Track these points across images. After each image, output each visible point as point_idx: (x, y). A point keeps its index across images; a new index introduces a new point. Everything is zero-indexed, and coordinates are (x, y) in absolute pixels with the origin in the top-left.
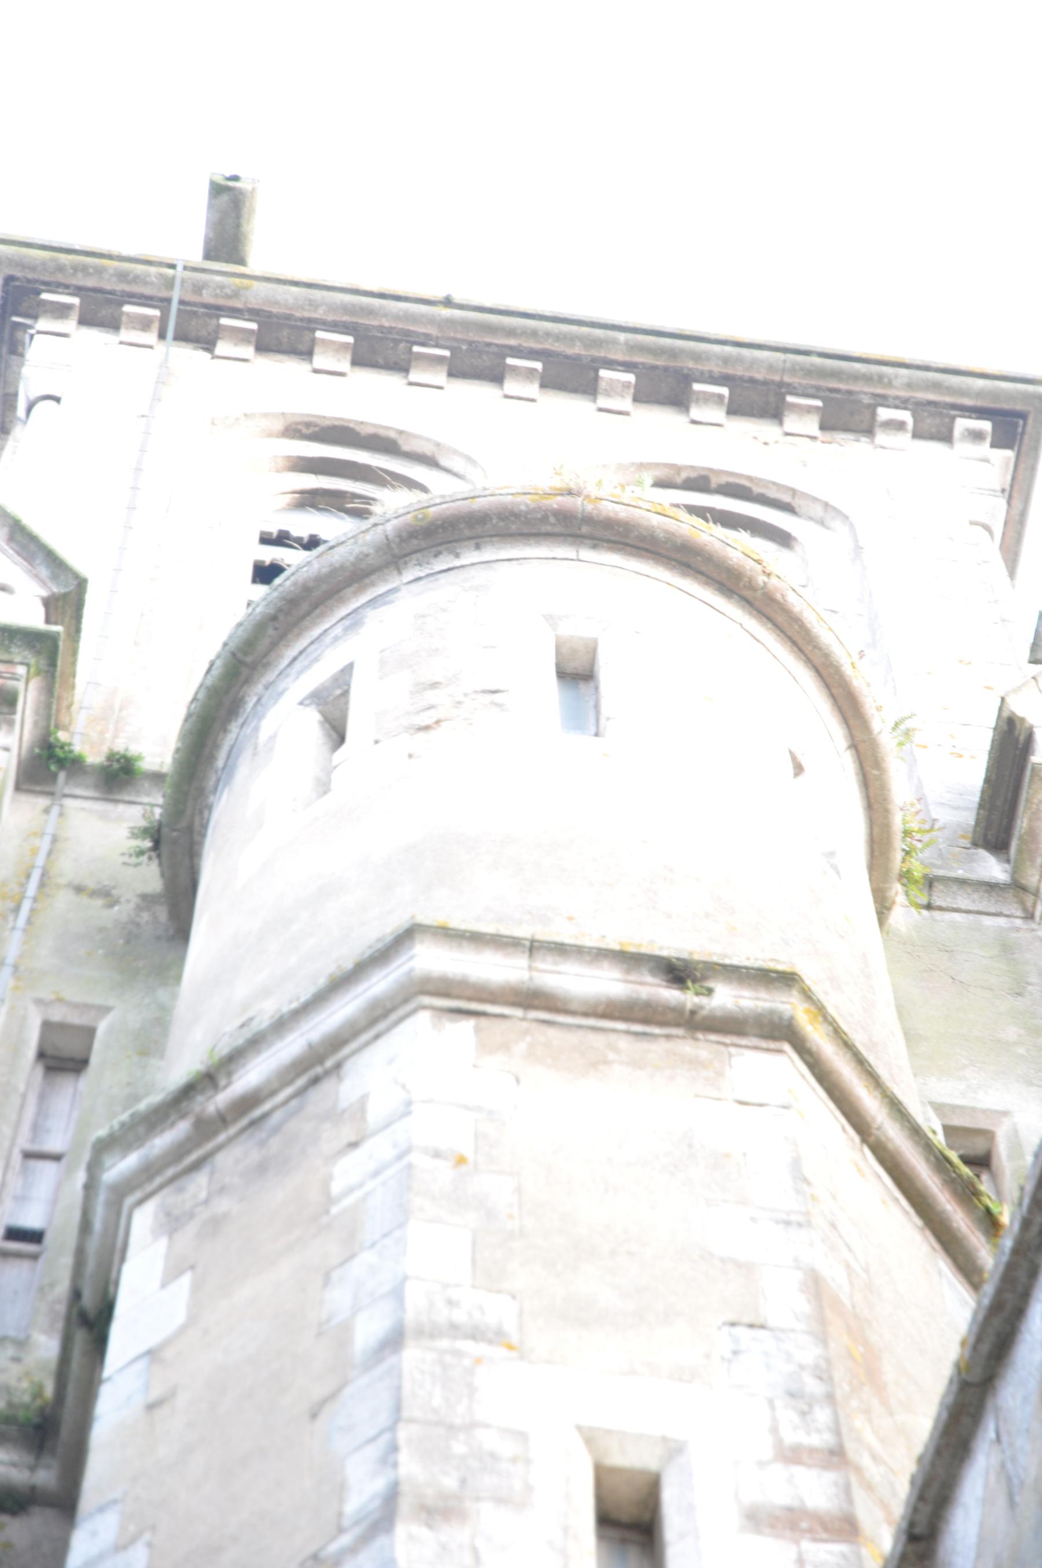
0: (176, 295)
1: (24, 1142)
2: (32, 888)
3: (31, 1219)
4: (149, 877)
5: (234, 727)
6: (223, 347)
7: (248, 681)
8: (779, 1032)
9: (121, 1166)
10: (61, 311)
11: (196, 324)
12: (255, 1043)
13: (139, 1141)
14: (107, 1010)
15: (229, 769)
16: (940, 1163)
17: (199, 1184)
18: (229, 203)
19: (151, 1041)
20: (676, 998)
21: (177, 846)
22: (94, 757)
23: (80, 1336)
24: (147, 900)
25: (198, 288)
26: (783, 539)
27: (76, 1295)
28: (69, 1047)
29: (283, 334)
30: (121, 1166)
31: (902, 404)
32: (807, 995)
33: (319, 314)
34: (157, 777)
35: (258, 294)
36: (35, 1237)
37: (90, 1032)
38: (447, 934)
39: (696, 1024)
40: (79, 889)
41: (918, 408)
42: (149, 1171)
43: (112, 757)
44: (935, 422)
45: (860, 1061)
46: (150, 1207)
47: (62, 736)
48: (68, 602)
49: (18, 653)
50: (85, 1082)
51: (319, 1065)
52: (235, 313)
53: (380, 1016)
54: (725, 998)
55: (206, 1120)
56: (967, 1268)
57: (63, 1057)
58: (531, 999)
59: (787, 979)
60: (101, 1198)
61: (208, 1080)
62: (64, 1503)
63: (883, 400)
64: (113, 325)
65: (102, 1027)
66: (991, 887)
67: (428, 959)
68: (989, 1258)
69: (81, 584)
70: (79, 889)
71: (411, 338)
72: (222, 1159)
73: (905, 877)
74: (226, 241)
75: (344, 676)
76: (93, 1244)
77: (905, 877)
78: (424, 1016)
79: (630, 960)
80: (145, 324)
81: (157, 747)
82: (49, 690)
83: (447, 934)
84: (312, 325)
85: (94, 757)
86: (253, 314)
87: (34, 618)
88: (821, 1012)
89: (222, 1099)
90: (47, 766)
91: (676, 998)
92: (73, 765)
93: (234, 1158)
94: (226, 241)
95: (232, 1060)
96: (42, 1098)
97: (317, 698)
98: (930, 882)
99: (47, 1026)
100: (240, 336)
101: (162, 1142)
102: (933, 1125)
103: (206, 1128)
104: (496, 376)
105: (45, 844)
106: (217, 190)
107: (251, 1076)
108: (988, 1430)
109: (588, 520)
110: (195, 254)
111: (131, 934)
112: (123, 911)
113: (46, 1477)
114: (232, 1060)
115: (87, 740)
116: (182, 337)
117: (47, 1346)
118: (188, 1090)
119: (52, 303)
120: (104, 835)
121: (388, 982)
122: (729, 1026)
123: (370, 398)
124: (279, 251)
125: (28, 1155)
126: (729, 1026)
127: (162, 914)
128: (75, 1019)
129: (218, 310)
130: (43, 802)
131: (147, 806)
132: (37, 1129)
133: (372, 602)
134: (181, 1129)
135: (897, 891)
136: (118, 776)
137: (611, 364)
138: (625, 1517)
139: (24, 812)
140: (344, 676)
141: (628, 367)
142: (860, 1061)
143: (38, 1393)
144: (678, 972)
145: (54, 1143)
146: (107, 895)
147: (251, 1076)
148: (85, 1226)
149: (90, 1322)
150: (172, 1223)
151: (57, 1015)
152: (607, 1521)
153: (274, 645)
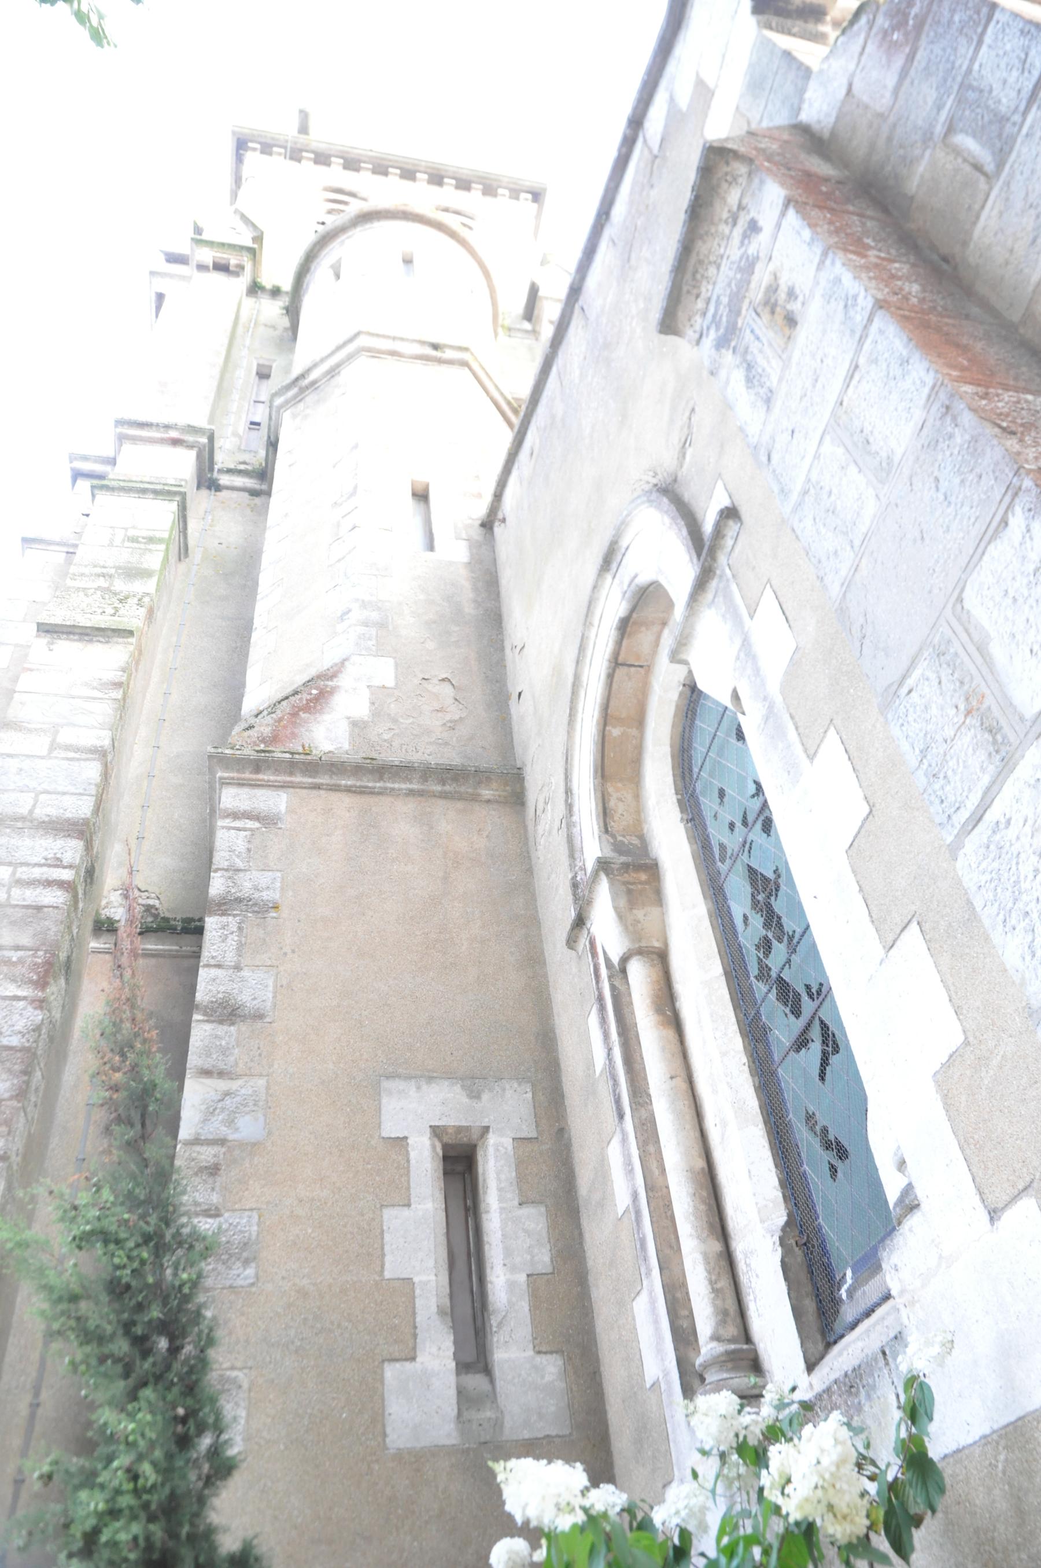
0: (289, 145)
1: (254, 398)
2: (252, 325)
3: (257, 420)
4: (286, 322)
5: (308, 276)
6: (303, 162)
7: (312, 262)
8: (464, 364)
9: (279, 401)
10: (254, 149)
11: (295, 155)
12: (315, 365)
13: (284, 394)
14: (275, 361)
15: (307, 288)
16: (509, 403)
17: (301, 406)
18: (304, 117)
19: (287, 370)
20: (435, 353)
21: (293, 311)
22: (269, 286)
23: (271, 449)
24: (286, 329)
25: (295, 143)
26: (470, 228)
27: (269, 437)
28: (265, 371)
29: (322, 159)
30: (279, 401)
31: (505, 188)
32: (472, 354)
33: (332, 153)
34: (287, 293)
35: (314, 146)
36: (259, 424)
37: (270, 367)
38: (369, 334)
39: (440, 361)
40: (266, 325)
41: (511, 190)
42: (287, 402)
43: (274, 286)
44: (515, 194)
45: (487, 374)
46: (289, 411)
47: (259, 280)
48: (259, 239)
49: (245, 253)
50: (270, 381)
51: (333, 372)
52: (307, 151)
53: (350, 357)
54: (449, 354)
55: (302, 387)
56: (510, 424)
57: (263, 375)
58: (393, 353)
59: (466, 349)
60: (274, 409)
61: (302, 376)
62: (268, 493)
63: (500, 187)
64: (270, 154)
65: (274, 366)
66: (527, 331)
67: (363, 341)
68: (516, 421)
69: (262, 233)
70: (266, 325)
71: (360, 161)
72: (307, 399)
73: (502, 326)
74: (304, 130)
75: (339, 261)
76: (273, 423)
77: (502, 326)
78: (363, 357)
79: (423, 343)
80: (280, 154)
81: (287, 286)
82: (254, 265)
83: (369, 334)
84: (330, 156)
85: (269, 286)
86: (313, 152)
87: (249, 243)
88: (476, 359)
89: (306, 382)
90: (255, 289)
91: (435, 353)
92: (262, 289)
93: (311, 398)
94: (304, 130)
95: (309, 371)
96: (258, 386)
97: (332, 267)
98: (510, 329)
99: (258, 365)
100: (309, 159)
101: (290, 394)
102: (509, 397)
103: (302, 390)
104: (386, 174)
105: (255, 312)
106: (301, 111)
107: (313, 376)
108: (516, 466)
109: (411, 214)
110: (295, 133)
111: (282, 339)
112: (278, 333)
113: (264, 487)
114: (309, 371)
115: (267, 281)
116: (291, 158)
117: (262, 453)
118: (297, 379)
119: (587, 1031)
120: (272, 310)
121: (353, 349)
122: (450, 362)
123: (348, 180)
124: (319, 137)
125: (255, 402)
126: (450, 362)
127: (290, 334)
128: (267, 363)
129: (301, 150)
130: (254, 300)
131: (283, 301)
132: (257, 394)
133: (348, 238)
134: (295, 390)
135: (500, 330)
136: (276, 292)
137: (420, 172)
138: (420, 493)
139: (249, 302)
140: (339, 261)
141: (425, 173)
142: (487, 374)
143: (261, 464)
144: (436, 347)
145: (262, 399)
146: (274, 327)
147: (313, 376)
148: (270, 418)
149: (273, 445)
150: (294, 416)
151: (261, 362)
152: (414, 495)
153: (319, 250)
